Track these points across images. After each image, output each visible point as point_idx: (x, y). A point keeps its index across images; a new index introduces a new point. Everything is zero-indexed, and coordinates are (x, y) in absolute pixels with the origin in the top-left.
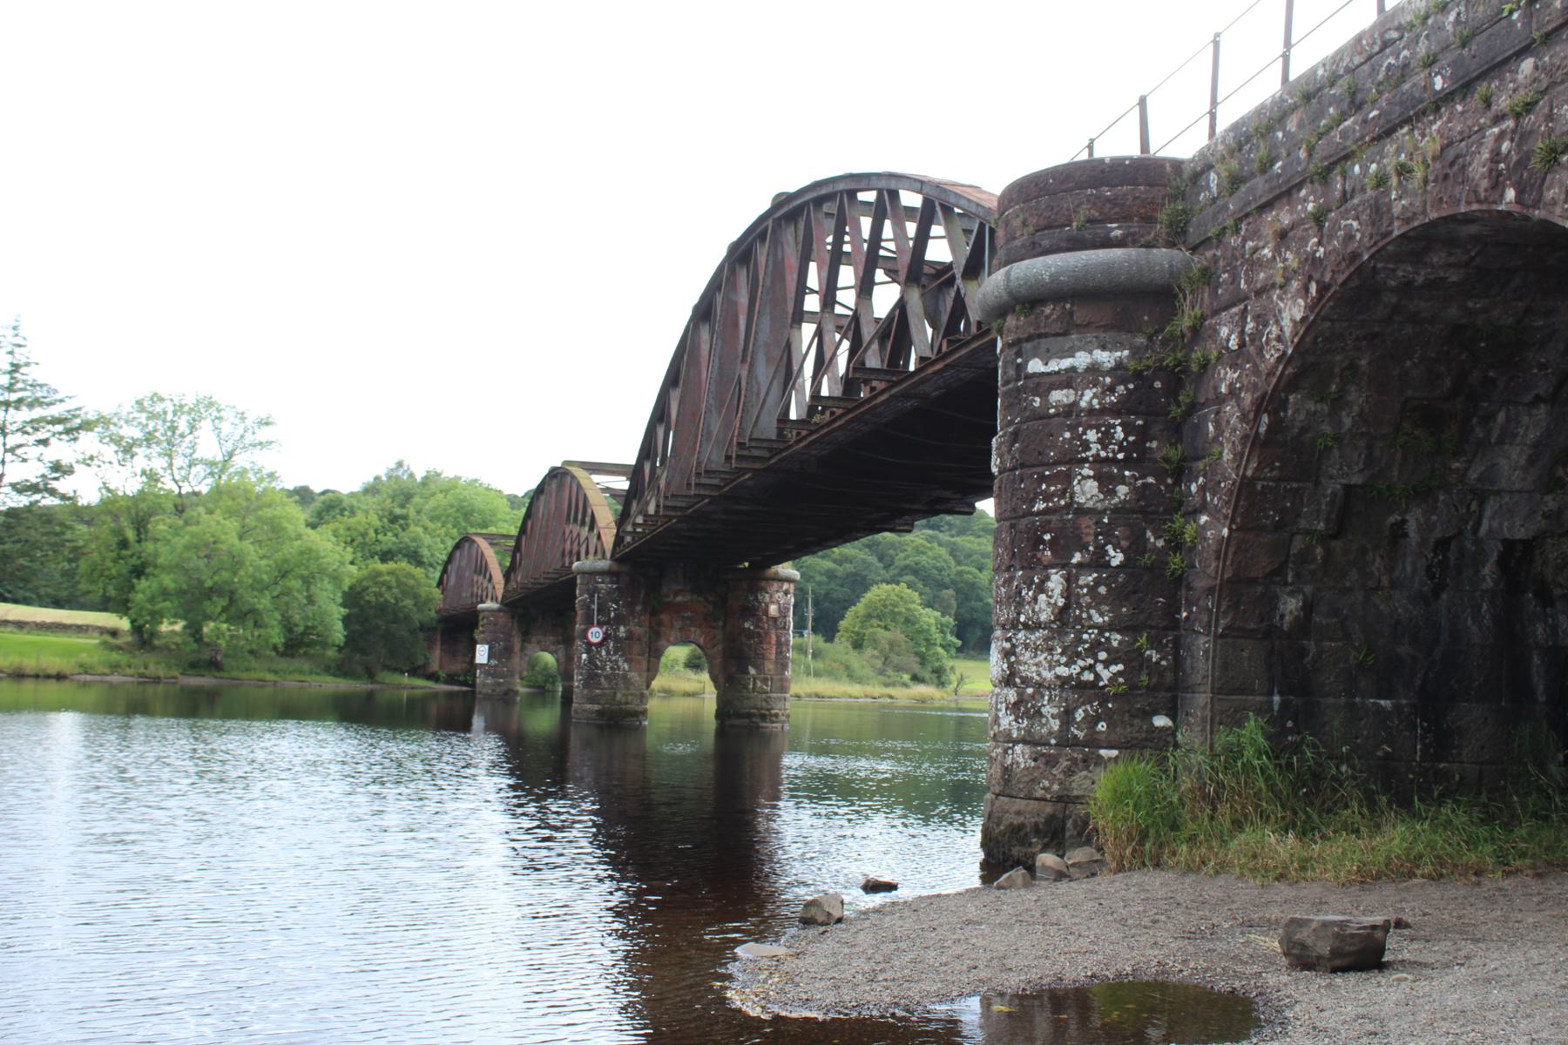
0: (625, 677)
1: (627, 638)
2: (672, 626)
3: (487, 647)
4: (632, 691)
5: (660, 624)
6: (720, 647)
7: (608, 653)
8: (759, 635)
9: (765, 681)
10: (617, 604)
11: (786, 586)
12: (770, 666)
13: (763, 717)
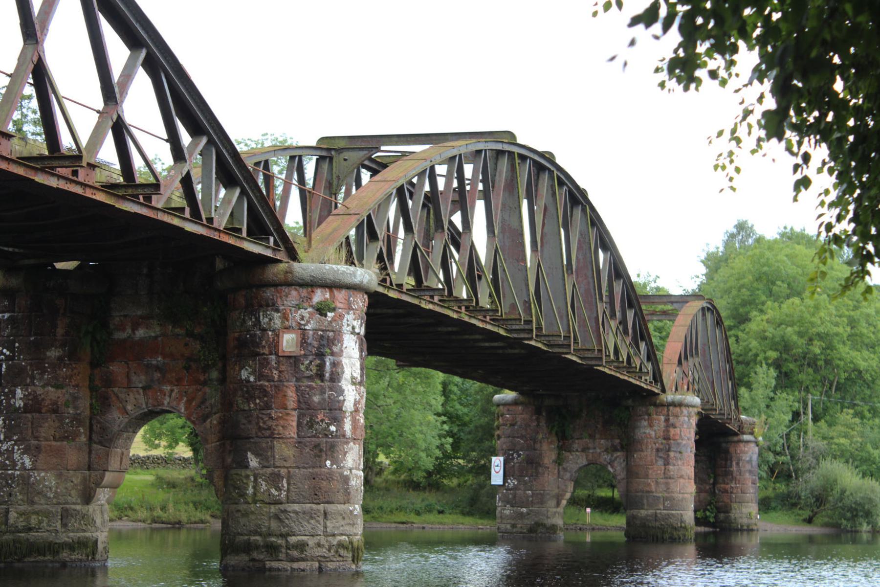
0: (25, 481)
1: (27, 409)
2: (129, 387)
4: (42, 505)
5: (109, 382)
6: (215, 420)
8: (264, 392)
9: (275, 480)
10: (11, 348)
11: (319, 296)
12: (284, 451)
13: (272, 550)
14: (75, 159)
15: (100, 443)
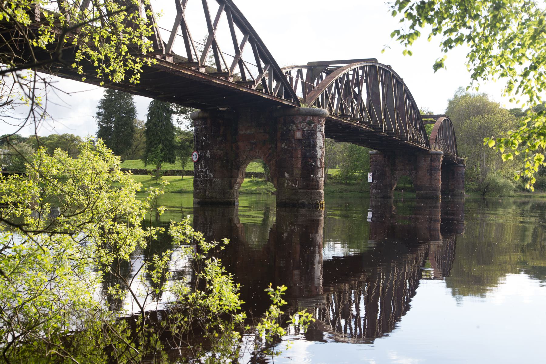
0: (211, 181)
3: (372, 173)
7: (201, 167)
10: (205, 137)
11: (309, 119)
14: (226, 75)
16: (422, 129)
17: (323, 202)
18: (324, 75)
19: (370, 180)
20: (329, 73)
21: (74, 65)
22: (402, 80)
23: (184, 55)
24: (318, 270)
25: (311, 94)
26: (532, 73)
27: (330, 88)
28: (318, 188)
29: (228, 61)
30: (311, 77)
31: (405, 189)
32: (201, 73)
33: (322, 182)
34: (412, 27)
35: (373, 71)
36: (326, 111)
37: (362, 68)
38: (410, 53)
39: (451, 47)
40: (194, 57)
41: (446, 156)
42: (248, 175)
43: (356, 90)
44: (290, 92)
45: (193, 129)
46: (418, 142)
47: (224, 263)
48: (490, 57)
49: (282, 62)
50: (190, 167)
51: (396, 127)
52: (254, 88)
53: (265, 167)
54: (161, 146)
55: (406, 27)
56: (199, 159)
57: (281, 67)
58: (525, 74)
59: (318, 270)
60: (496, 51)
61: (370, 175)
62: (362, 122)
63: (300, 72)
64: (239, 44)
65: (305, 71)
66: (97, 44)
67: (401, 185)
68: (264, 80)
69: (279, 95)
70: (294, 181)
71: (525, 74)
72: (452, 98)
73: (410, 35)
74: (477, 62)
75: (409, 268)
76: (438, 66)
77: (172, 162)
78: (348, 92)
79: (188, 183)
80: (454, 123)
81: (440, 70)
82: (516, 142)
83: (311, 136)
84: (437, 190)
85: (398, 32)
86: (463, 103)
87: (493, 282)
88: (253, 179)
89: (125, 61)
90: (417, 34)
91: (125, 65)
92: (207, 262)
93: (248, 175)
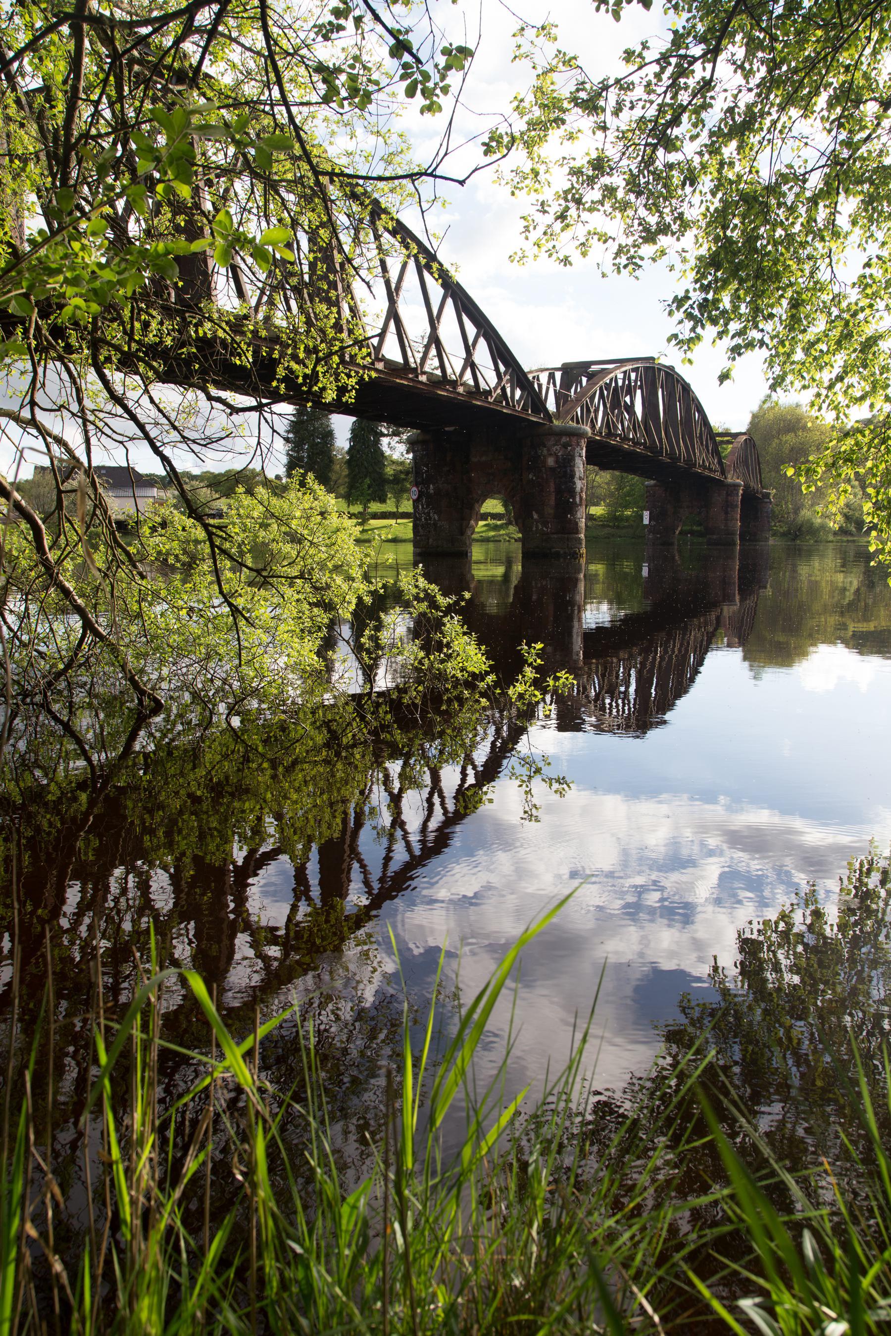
0: (435, 524)
11: (564, 439)
14: (454, 384)
15: (43, 469)
16: (716, 453)
17: (583, 550)
18: (584, 380)
19: (646, 521)
20: (591, 376)
21: (274, 384)
22: (688, 385)
23: (399, 359)
24: (578, 644)
25: (568, 406)
26: (839, 385)
27: (592, 398)
28: (577, 532)
29: (455, 362)
30: (567, 383)
31: (692, 533)
32: (421, 383)
33: (582, 523)
34: (693, 329)
35: (650, 373)
36: (588, 429)
37: (635, 370)
38: (690, 361)
39: (740, 354)
40: (411, 360)
41: (747, 487)
42: (484, 517)
43: (628, 399)
44: (536, 401)
45: (411, 456)
46: (710, 470)
47: (464, 622)
48: (793, 363)
49: (527, 364)
50: (407, 506)
51: (682, 449)
52: (491, 400)
53: (505, 505)
54: (368, 481)
55: (686, 328)
56: (420, 497)
57: (526, 370)
58: (830, 387)
59: (578, 644)
60: (799, 355)
61: (646, 515)
62: (636, 443)
63: (552, 377)
64: (471, 341)
65: (558, 375)
66: (302, 355)
67: (687, 528)
68: (504, 389)
69: (524, 408)
70: (545, 524)
71: (830, 387)
72: (755, 409)
73: (690, 340)
74: (777, 370)
75: (694, 635)
76: (724, 377)
77: (383, 500)
78: (616, 402)
79: (405, 528)
80: (758, 443)
81: (727, 383)
82: (819, 470)
83: (567, 463)
84: (734, 534)
85: (675, 336)
86: (770, 416)
87: (802, 653)
88: (490, 521)
89: (337, 375)
90: (698, 338)
91: (337, 380)
92: (445, 620)
93: (484, 517)
